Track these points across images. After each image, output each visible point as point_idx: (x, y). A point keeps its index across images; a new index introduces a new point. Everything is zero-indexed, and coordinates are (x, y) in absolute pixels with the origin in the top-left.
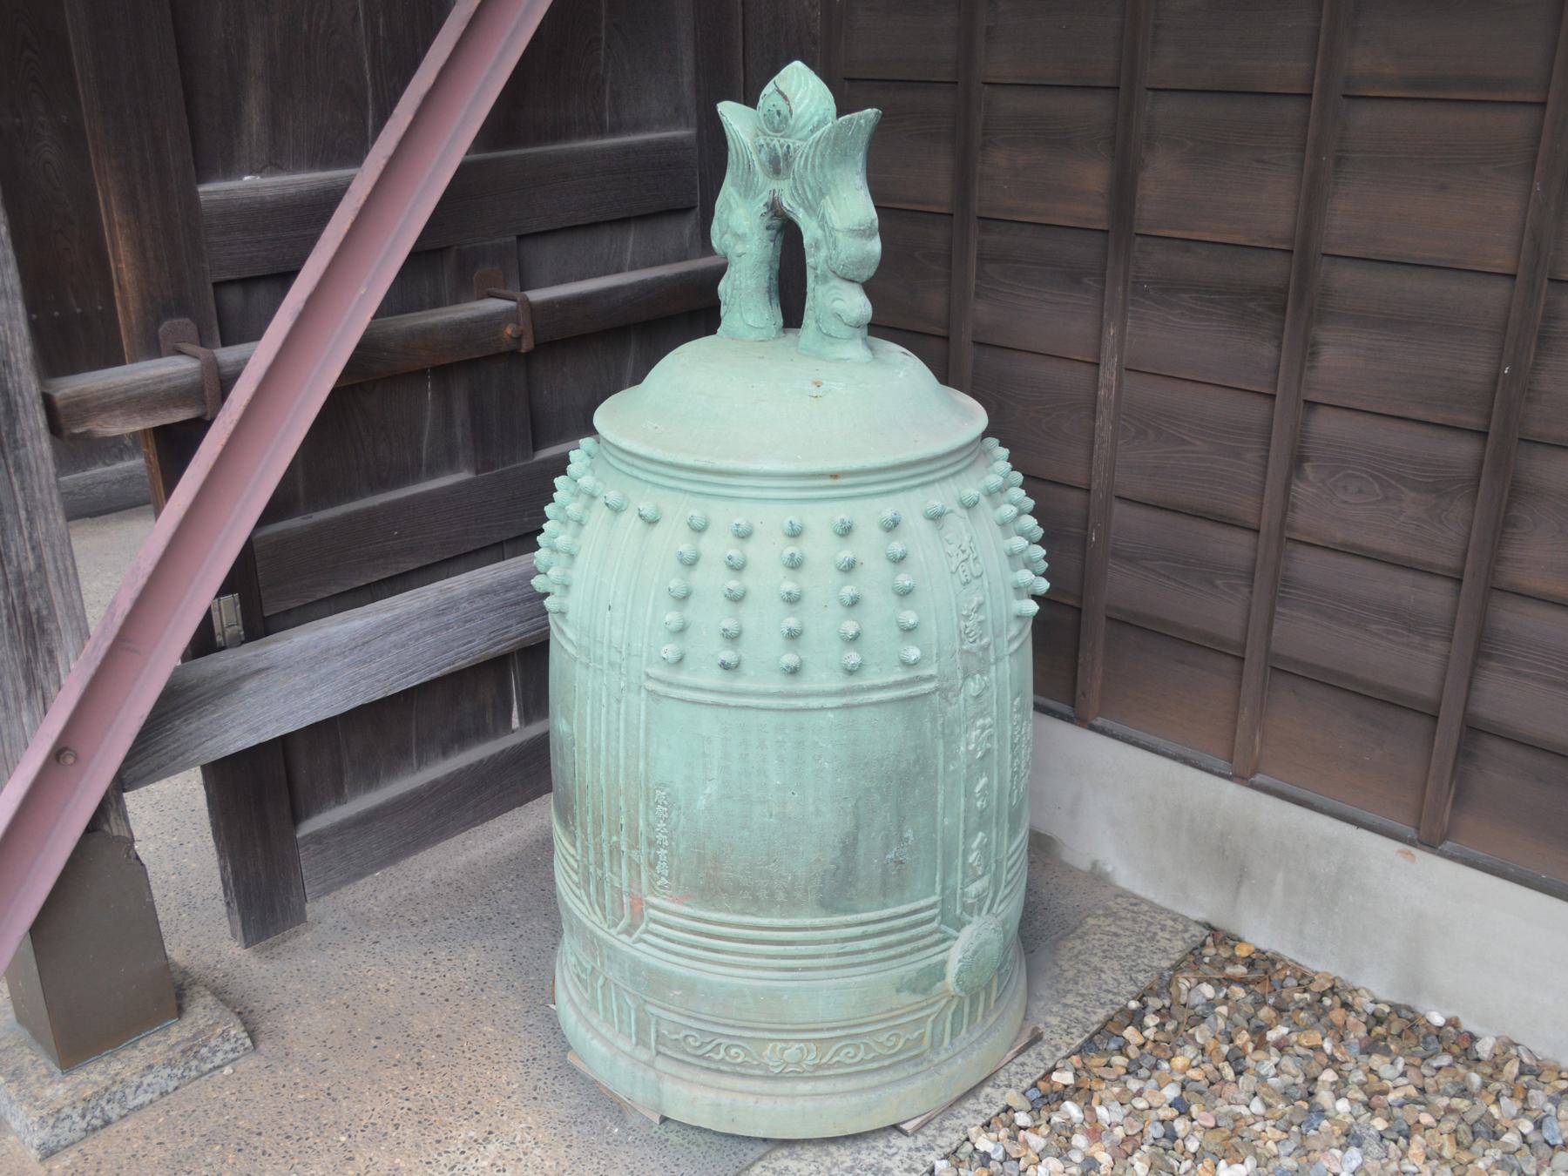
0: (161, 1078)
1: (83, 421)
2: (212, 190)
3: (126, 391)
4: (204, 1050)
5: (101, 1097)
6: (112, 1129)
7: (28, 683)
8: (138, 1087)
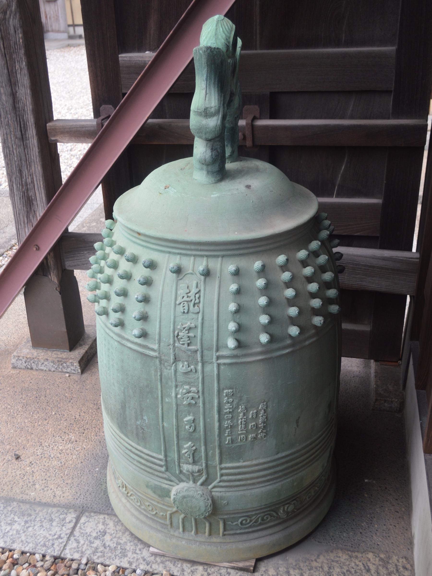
0: (50, 365)
1: (54, 136)
2: (124, 57)
3: (70, 128)
4: (65, 364)
5: (31, 360)
6: (32, 371)
7: (27, 219)
8: (42, 364)
